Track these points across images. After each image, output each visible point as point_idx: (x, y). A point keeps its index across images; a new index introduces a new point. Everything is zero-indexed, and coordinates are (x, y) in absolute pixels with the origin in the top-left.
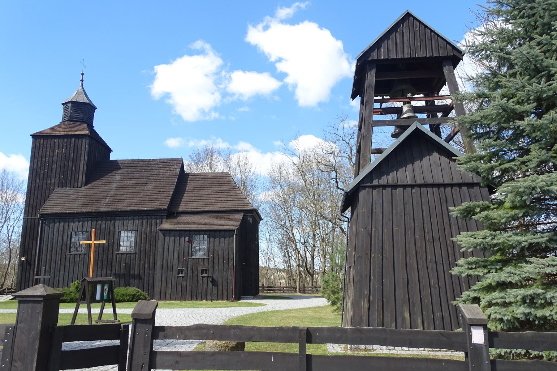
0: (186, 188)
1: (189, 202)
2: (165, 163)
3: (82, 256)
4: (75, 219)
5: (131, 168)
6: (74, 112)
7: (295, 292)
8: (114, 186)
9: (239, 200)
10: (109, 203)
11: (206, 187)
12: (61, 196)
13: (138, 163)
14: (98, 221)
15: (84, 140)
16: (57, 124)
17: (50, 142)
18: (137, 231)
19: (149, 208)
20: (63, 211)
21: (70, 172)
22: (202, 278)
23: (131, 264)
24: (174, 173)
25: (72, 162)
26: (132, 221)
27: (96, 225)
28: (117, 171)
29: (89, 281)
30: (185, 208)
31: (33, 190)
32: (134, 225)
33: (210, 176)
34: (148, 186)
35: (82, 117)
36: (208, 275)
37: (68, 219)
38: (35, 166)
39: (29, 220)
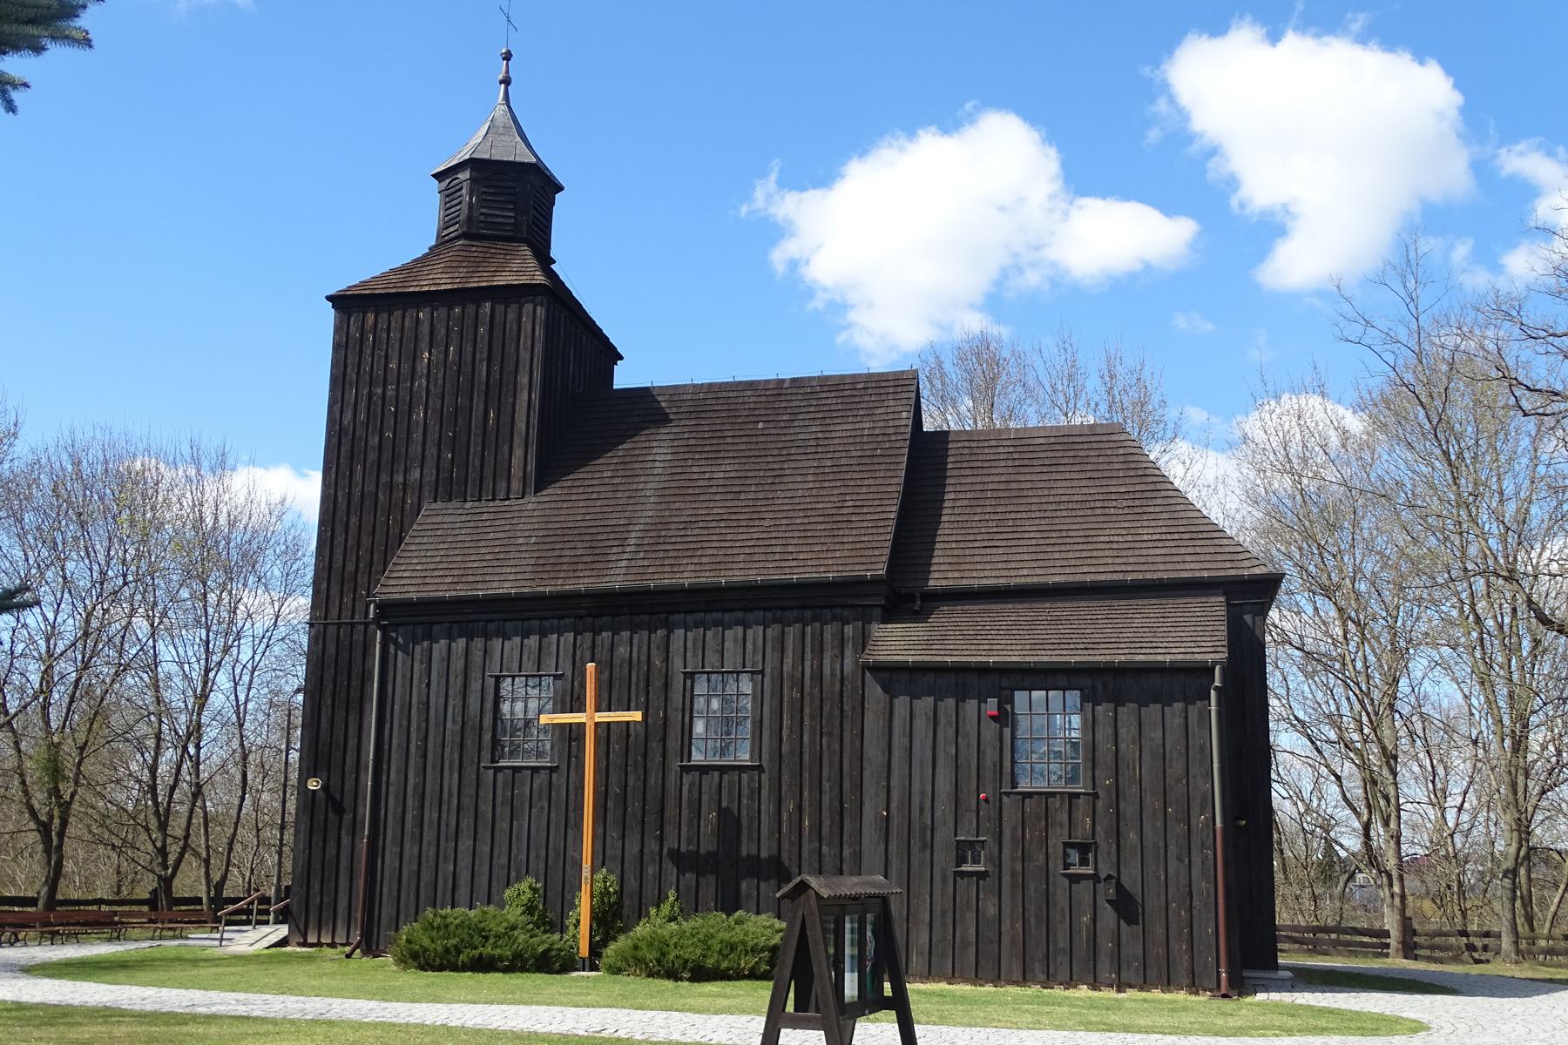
0: (944, 493)
1: (968, 552)
2: (847, 393)
3: (544, 775)
4: (507, 624)
5: (708, 415)
6: (481, 201)
7: (1382, 950)
8: (650, 488)
9: (1195, 536)
10: (641, 555)
11: (1029, 485)
12: (449, 532)
13: (735, 394)
14: (601, 630)
15: (528, 307)
16: (408, 259)
17: (400, 320)
18: (762, 672)
19: (811, 574)
20: (462, 591)
21: (476, 439)
22: (1067, 882)
23: (744, 812)
24: (892, 431)
25: (483, 395)
26: (740, 629)
27: (593, 647)
28: (653, 431)
29: (825, 893)
30: (956, 575)
31: (341, 513)
32: (749, 647)
33: (1042, 441)
34: (790, 486)
35: (513, 221)
36: (1096, 869)
37: (481, 624)
38: (348, 418)
39: (332, 630)
